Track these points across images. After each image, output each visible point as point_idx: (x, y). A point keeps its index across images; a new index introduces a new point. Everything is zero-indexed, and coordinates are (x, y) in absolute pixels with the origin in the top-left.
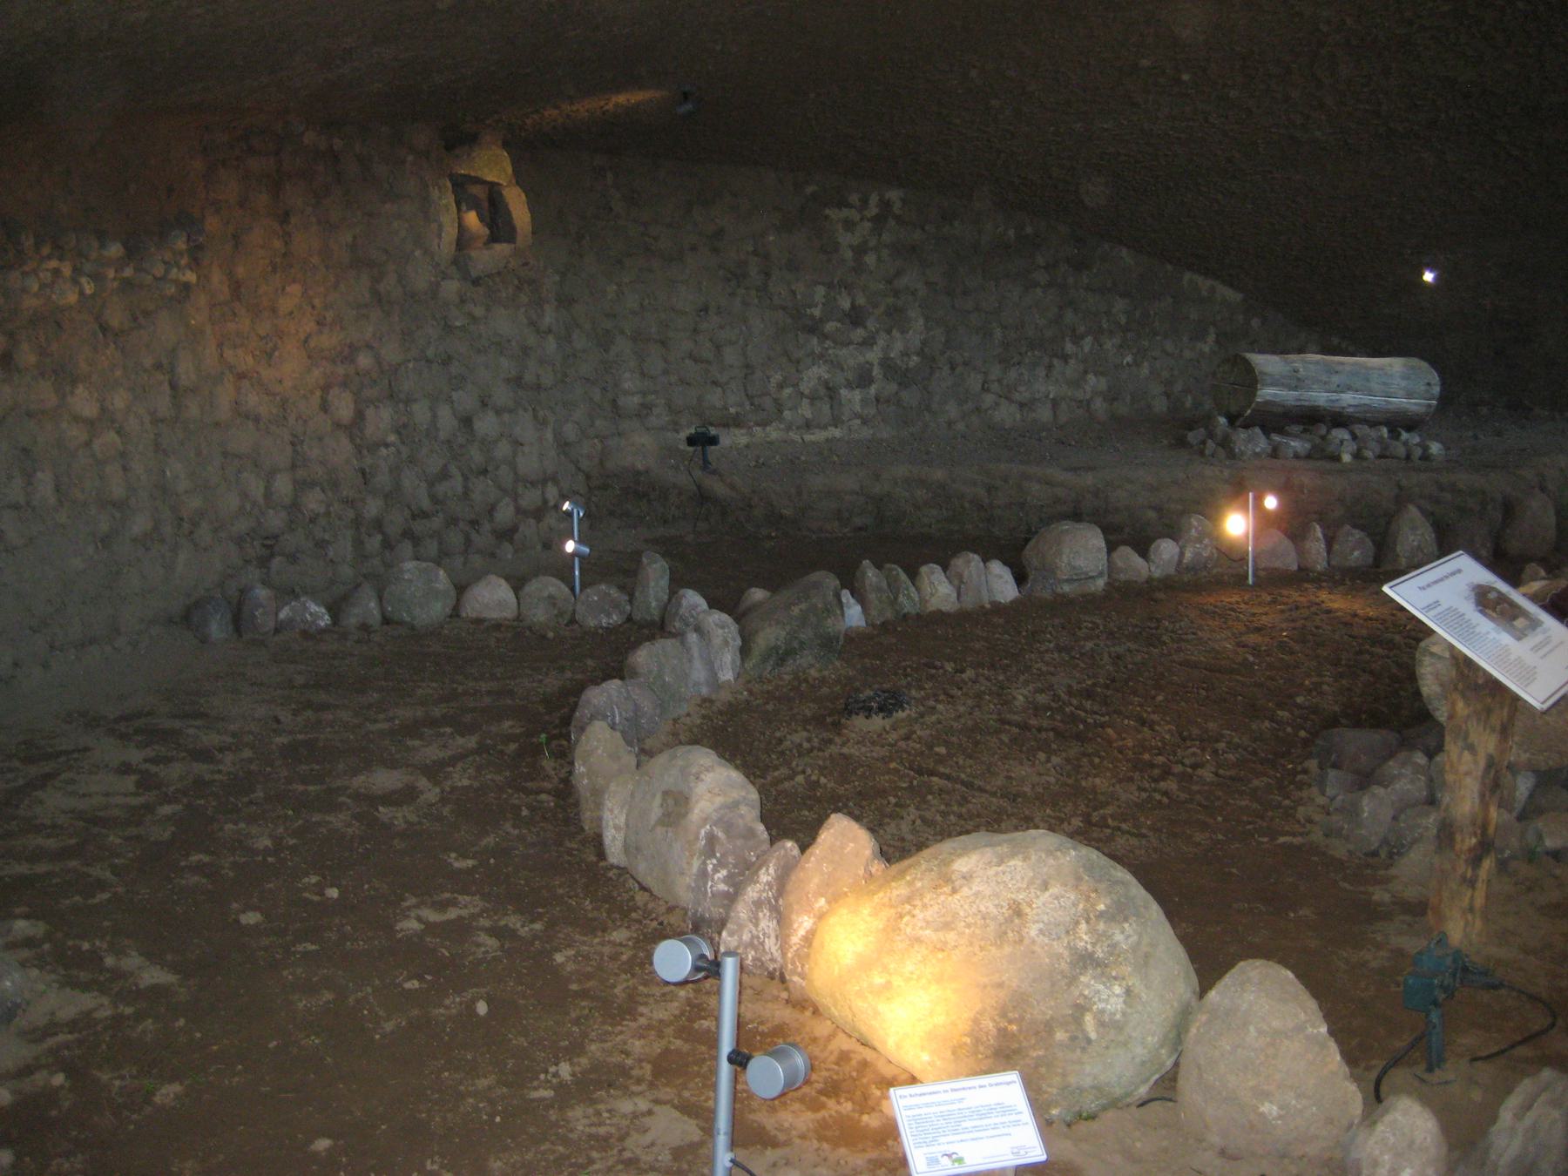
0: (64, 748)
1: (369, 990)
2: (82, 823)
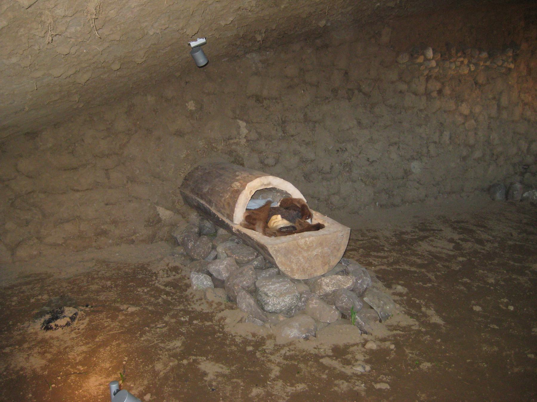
0: (434, 228)
1: (513, 352)
2: (431, 257)
